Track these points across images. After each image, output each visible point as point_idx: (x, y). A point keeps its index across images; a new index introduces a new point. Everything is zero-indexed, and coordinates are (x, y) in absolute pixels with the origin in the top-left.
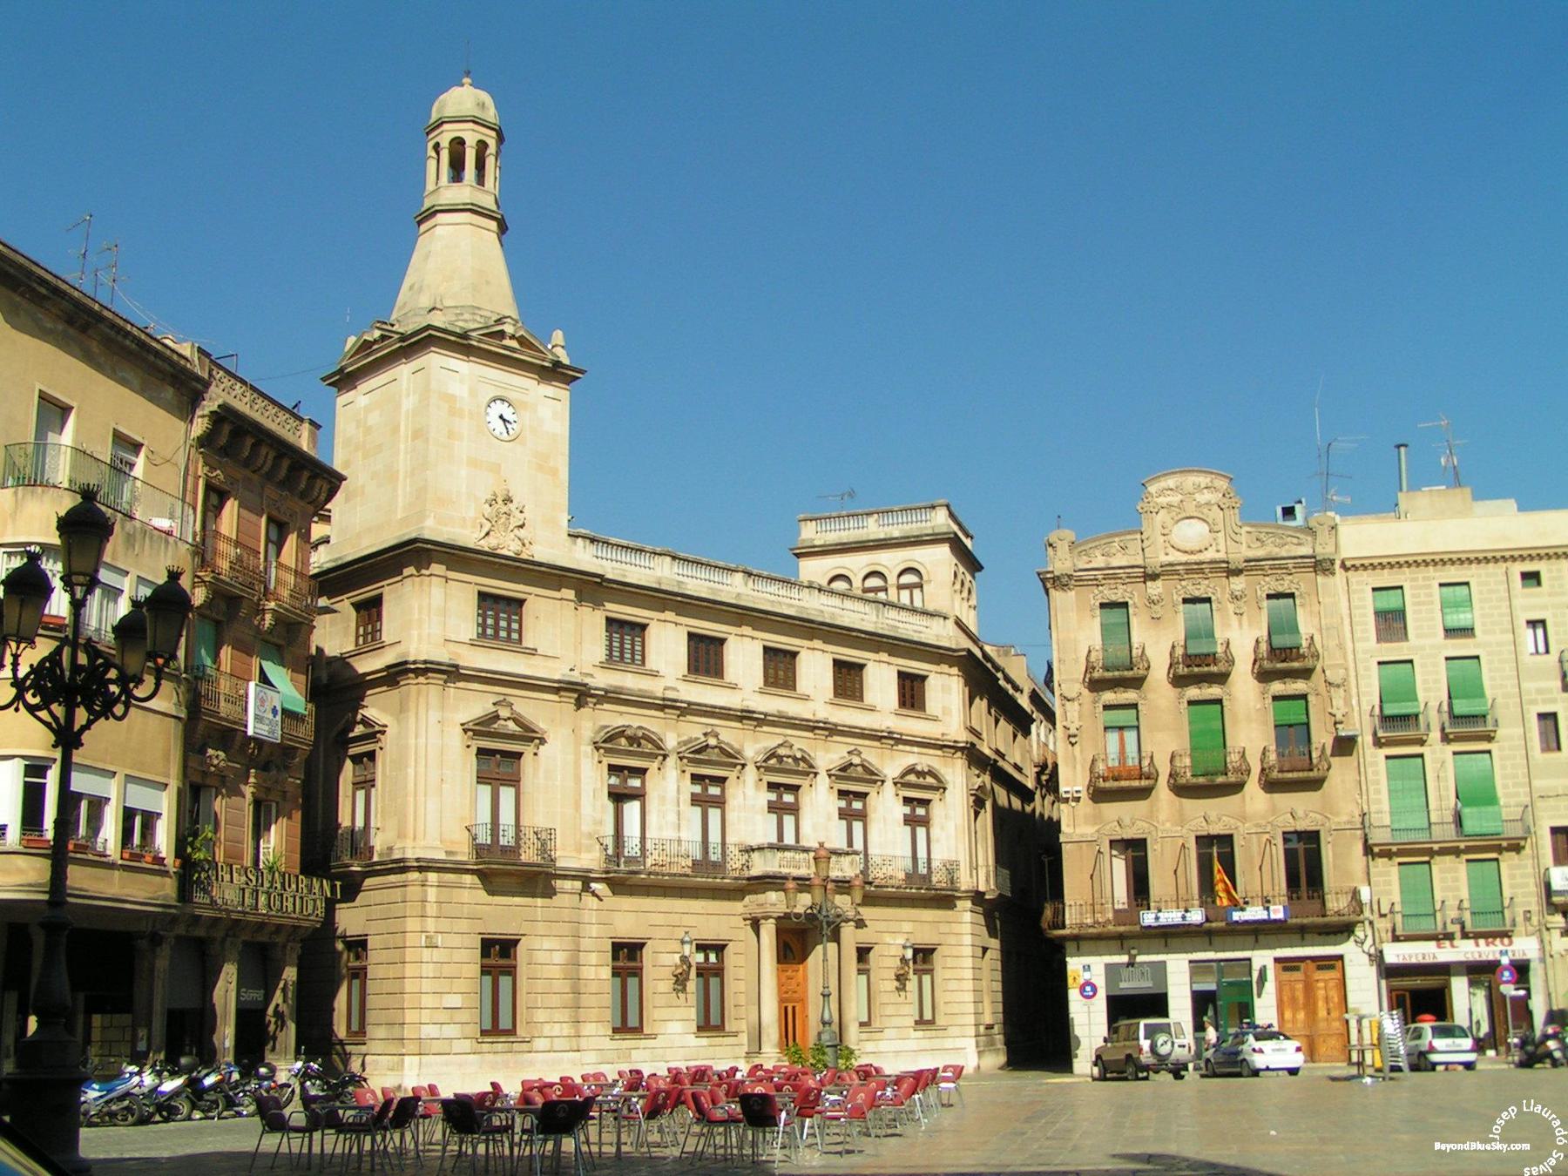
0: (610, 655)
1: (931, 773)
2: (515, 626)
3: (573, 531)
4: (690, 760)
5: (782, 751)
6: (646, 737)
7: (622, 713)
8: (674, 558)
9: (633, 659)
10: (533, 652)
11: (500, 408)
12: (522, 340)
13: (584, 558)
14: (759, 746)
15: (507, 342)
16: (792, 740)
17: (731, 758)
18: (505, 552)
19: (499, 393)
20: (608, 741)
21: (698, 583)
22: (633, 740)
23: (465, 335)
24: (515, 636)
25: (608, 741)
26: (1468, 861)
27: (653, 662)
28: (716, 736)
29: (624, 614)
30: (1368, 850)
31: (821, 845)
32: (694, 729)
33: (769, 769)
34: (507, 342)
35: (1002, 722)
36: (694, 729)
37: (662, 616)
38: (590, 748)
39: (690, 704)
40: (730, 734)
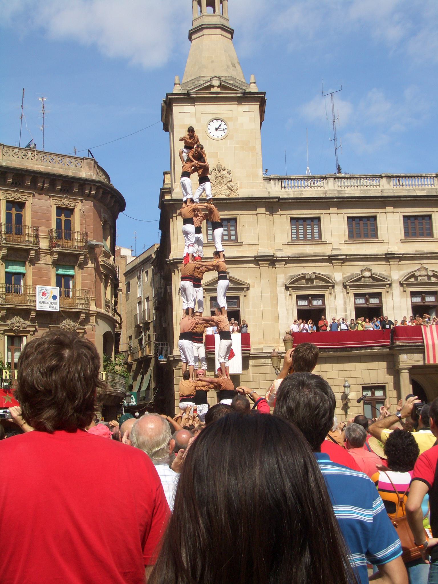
0: (298, 237)
1: (319, 278)
2: (233, 232)
3: (267, 177)
4: (351, 286)
5: (417, 274)
6: (317, 278)
7: (304, 267)
8: (335, 178)
9: (313, 237)
10: (241, 244)
11: (216, 124)
12: (220, 86)
13: (275, 190)
14: (402, 273)
15: (212, 90)
16: (426, 266)
17: (380, 281)
18: (221, 196)
19: (214, 116)
20: (292, 285)
21: (352, 190)
22: (311, 280)
23: (188, 94)
24: (233, 237)
25: (292, 285)
26: (294, 220)
27: (326, 236)
28: (370, 270)
29: (305, 212)
30: (262, 102)
31: (274, 350)
32: (354, 269)
33: (409, 285)
34: (212, 90)
35: (84, 201)
36: (354, 269)
37: (327, 211)
38: (283, 288)
39: (346, 256)
40: (379, 269)
